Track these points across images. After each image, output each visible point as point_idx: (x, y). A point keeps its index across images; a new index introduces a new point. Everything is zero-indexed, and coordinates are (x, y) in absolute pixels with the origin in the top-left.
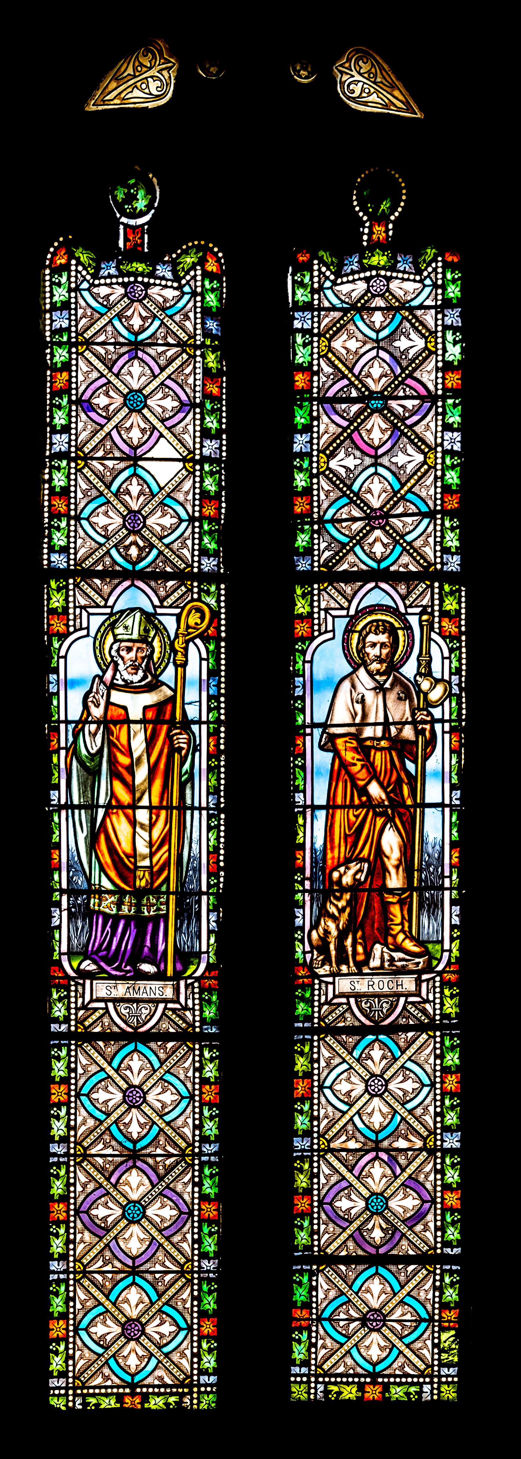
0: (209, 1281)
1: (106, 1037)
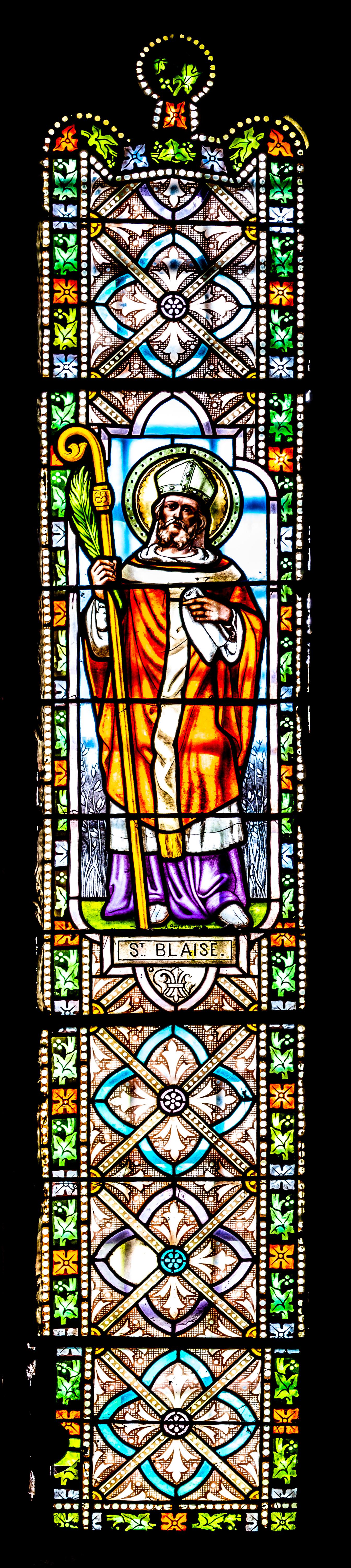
0: (286, 1438)
1: (130, 1020)
